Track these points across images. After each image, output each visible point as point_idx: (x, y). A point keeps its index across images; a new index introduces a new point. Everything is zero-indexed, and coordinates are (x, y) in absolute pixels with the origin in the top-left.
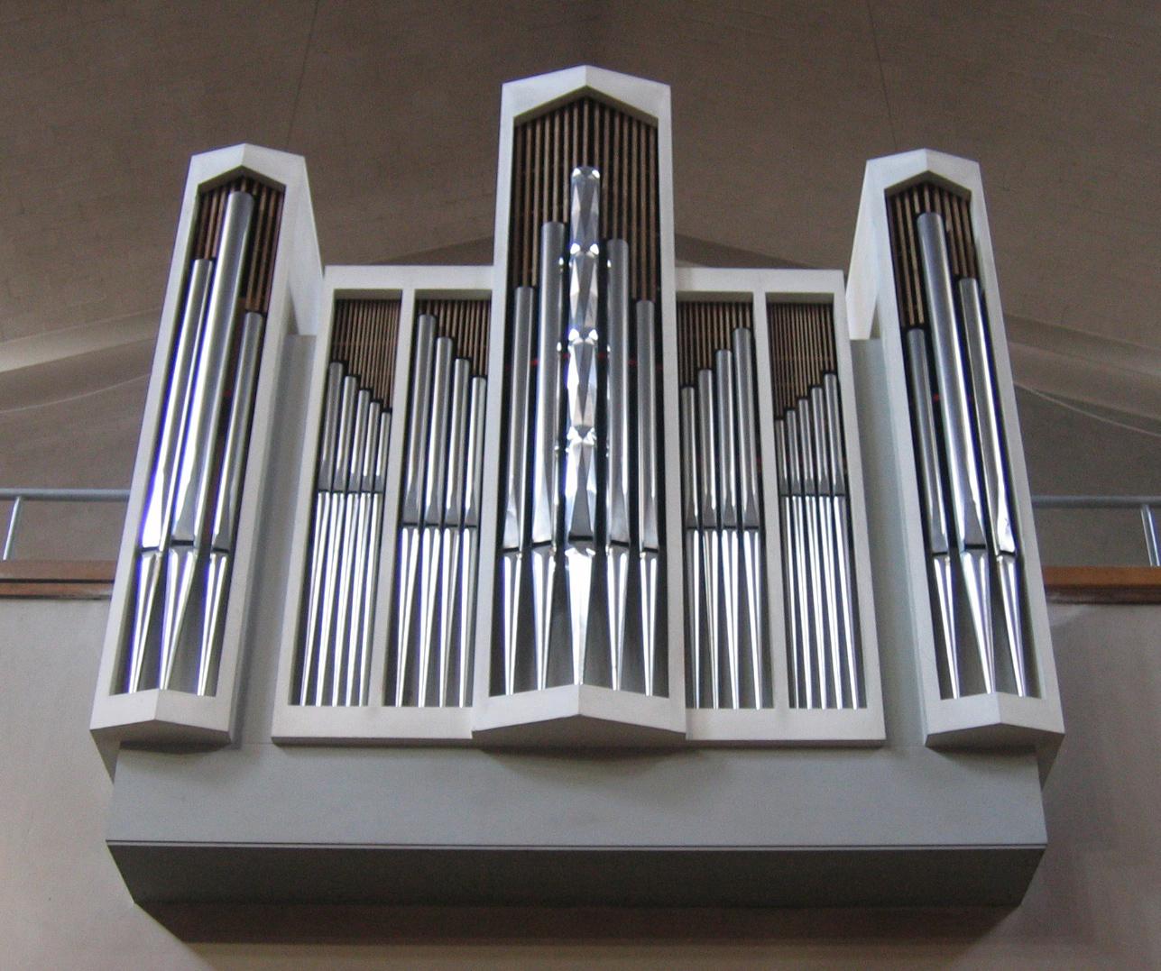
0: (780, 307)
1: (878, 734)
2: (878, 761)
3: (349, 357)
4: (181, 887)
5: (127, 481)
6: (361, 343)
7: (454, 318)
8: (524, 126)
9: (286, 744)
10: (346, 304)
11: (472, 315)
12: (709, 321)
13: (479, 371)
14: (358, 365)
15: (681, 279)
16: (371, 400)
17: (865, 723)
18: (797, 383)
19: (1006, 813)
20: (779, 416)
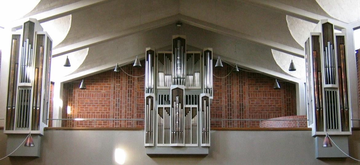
0: (195, 54)
1: (198, 146)
2: (197, 148)
3: (166, 113)
4: (152, 156)
5: (295, 96)
6: (160, 111)
7: (167, 109)
8: (172, 90)
9: (158, 147)
10: (159, 108)
11: (169, 109)
12: (187, 110)
13: (169, 115)
14: (160, 114)
15: (185, 106)
16: (160, 116)
17: (196, 145)
18: (342, 41)
19: (206, 152)
20: (195, 64)
